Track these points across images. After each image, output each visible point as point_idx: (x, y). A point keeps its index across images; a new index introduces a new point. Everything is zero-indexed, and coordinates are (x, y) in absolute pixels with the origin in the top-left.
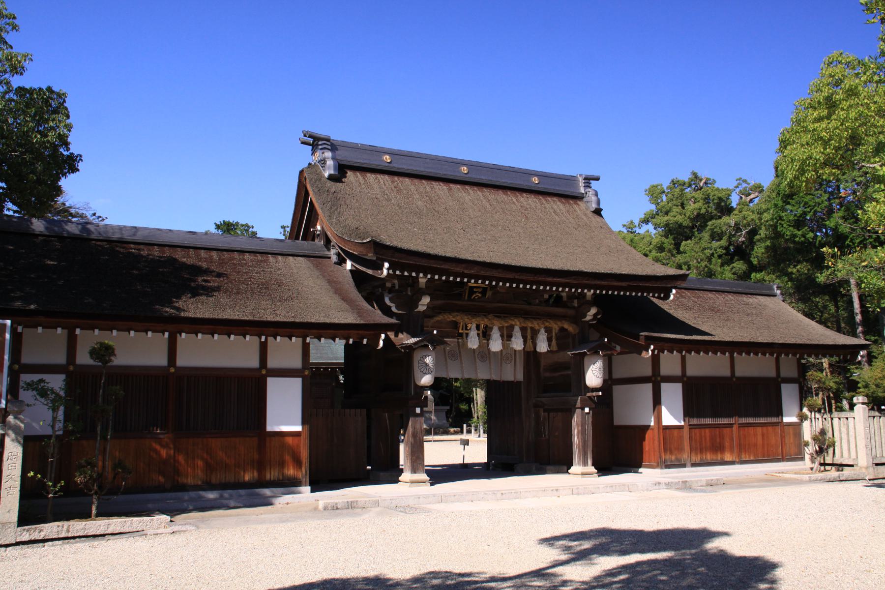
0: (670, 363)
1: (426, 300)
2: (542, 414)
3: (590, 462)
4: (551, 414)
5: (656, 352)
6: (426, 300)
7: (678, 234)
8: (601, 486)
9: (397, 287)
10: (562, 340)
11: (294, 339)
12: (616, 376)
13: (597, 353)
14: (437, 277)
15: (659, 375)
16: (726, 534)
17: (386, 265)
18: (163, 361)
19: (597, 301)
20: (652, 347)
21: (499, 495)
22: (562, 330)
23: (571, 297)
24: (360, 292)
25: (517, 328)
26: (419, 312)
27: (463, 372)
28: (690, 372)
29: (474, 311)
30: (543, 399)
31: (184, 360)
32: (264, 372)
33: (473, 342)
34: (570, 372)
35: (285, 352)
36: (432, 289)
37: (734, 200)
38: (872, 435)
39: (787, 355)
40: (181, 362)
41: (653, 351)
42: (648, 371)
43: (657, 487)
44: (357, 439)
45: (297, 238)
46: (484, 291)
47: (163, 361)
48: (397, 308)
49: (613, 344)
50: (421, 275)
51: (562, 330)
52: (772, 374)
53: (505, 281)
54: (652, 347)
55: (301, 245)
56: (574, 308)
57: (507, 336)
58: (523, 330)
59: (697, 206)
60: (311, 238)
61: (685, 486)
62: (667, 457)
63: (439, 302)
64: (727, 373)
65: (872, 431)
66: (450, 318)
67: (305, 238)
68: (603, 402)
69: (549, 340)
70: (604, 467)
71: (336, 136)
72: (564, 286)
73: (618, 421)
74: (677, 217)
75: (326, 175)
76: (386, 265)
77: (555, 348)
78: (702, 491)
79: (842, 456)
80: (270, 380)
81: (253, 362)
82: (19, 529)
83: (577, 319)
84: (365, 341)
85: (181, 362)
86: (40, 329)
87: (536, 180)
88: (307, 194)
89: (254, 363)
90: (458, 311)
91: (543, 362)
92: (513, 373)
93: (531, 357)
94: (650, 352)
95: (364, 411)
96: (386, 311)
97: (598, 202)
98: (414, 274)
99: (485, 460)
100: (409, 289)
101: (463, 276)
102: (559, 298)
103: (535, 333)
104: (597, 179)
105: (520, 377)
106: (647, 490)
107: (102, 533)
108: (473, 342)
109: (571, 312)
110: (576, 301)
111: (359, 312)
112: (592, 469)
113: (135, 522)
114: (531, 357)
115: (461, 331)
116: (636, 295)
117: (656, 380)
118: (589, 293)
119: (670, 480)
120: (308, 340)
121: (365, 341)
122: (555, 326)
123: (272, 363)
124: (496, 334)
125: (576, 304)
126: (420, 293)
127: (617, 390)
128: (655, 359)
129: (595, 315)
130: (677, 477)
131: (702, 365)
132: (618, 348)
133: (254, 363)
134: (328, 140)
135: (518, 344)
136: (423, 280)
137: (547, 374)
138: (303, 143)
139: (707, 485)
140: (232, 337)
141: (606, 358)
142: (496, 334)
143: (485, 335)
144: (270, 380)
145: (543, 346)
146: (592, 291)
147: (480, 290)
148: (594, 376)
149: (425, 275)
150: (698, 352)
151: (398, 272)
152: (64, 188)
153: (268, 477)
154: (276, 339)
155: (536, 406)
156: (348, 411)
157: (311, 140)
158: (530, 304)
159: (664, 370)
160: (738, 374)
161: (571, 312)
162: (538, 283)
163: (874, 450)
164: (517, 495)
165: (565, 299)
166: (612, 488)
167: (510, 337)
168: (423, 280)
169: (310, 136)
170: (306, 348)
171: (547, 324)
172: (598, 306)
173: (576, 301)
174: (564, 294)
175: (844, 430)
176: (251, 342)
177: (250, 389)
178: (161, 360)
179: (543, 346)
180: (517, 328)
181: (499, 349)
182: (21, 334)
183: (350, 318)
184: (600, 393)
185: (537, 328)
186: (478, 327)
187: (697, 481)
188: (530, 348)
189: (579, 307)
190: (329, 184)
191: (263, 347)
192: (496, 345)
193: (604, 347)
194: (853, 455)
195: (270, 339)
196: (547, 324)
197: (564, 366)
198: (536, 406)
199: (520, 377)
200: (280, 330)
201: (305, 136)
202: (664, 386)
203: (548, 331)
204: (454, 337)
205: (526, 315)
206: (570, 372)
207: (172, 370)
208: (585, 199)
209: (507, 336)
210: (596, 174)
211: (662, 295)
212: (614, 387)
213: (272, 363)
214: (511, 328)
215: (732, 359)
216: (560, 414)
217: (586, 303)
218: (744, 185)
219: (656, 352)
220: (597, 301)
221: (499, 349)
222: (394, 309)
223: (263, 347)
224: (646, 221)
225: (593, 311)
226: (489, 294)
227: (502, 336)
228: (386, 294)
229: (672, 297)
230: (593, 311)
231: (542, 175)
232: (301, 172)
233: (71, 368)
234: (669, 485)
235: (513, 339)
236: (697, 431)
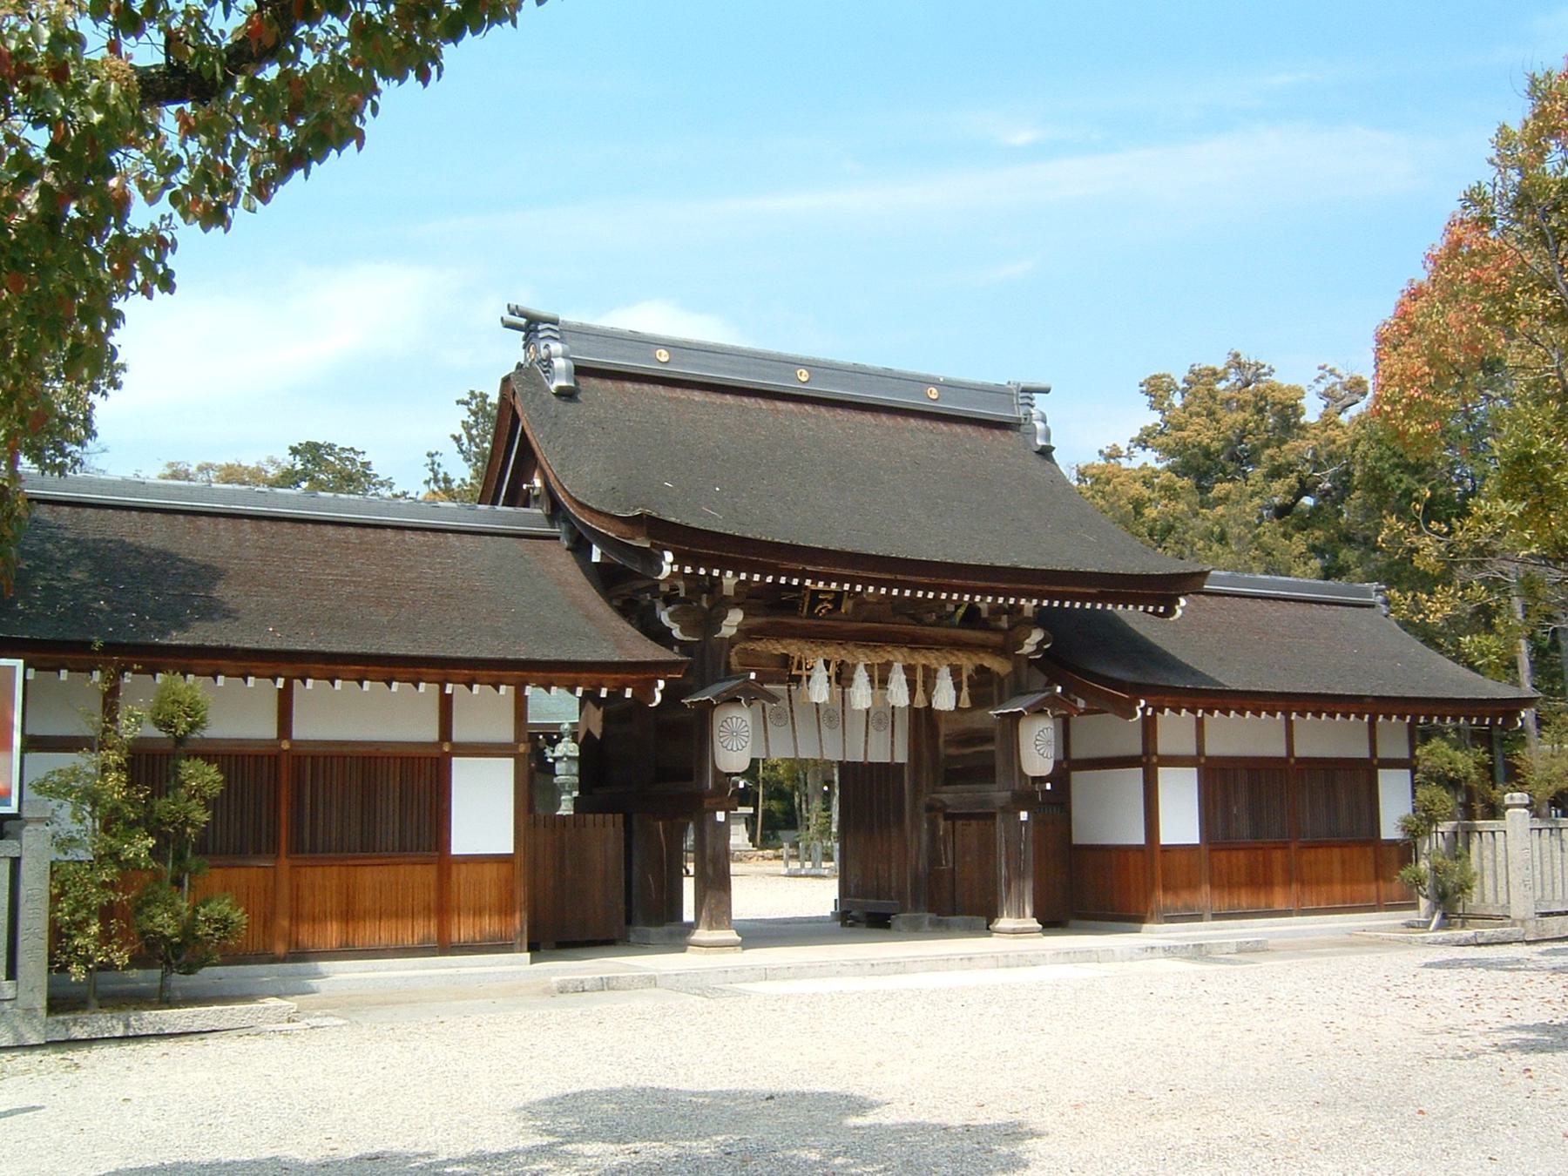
0: (1175, 732)
1: (735, 617)
2: (942, 823)
3: (1028, 911)
4: (959, 823)
5: (1149, 713)
6: (735, 617)
7: (1201, 468)
8: (1048, 954)
9: (682, 594)
10: (982, 688)
11: (422, 686)
12: (1078, 753)
13: (1042, 712)
17: (669, 557)
18: (269, 730)
19: (1042, 618)
20: (1143, 703)
21: (867, 967)
22: (981, 670)
23: (996, 611)
24: (609, 599)
25: (898, 667)
26: (723, 639)
28: (1211, 749)
29: (818, 636)
30: (944, 797)
31: (306, 729)
32: (446, 748)
33: (819, 690)
34: (991, 748)
35: (484, 712)
36: (746, 597)
37: (1312, 409)
38: (1537, 863)
39: (1388, 717)
41: (1144, 710)
42: (1136, 748)
43: (1148, 954)
44: (616, 865)
45: (494, 502)
46: (838, 597)
47: (269, 730)
48: (682, 631)
49: (1073, 696)
50: (729, 574)
51: (981, 670)
52: (1364, 753)
53: (878, 584)
54: (1143, 703)
55: (502, 515)
56: (1001, 630)
57: (881, 680)
58: (909, 670)
59: (1239, 417)
60: (521, 502)
61: (1199, 953)
62: (1169, 902)
63: (759, 621)
64: (1281, 751)
65: (1537, 854)
66: (778, 648)
67: (510, 502)
68: (1053, 799)
69: (958, 687)
70: (1053, 920)
71: (569, 316)
72: (984, 592)
73: (1077, 839)
74: (1202, 433)
75: (553, 387)
76: (669, 557)
77: (966, 703)
78: (1229, 962)
79: (1483, 901)
81: (428, 732)
82: (50, 1020)
83: (1007, 649)
84: (628, 693)
86: (64, 674)
87: (933, 393)
88: (516, 420)
89: (431, 733)
90: (793, 636)
91: (944, 729)
92: (887, 748)
93: (923, 720)
94: (1139, 713)
95: (620, 818)
96: (661, 636)
97: (1047, 436)
98: (716, 573)
100: (705, 596)
101: (803, 575)
102: (973, 609)
103: (930, 676)
104: (1046, 391)
105: (902, 757)
106: (1131, 959)
107: (185, 1029)
108: (819, 690)
109: (995, 638)
110: (1005, 617)
111: (619, 645)
112: (1033, 923)
113: (236, 1012)
114: (923, 720)
115: (794, 672)
117: (1148, 762)
118: (1029, 605)
119: (1173, 943)
120: (449, 689)
121: (628, 693)
122: (968, 663)
123: (459, 734)
124: (861, 677)
125: (1004, 622)
126: (722, 605)
127: (1081, 781)
128: (1149, 726)
129: (1040, 644)
130: (1186, 938)
131: (1244, 736)
132: (1081, 704)
133: (431, 733)
134: (555, 322)
135: (898, 693)
137: (952, 751)
138: (509, 326)
139: (1239, 951)
140: (310, 682)
141: (1060, 720)
142: (861, 677)
143: (842, 678)
145: (945, 698)
146: (1035, 602)
147: (830, 597)
148: (1037, 751)
149: (736, 574)
150: (1241, 712)
151: (688, 570)
152: (98, 422)
153: (455, 938)
154: (417, 687)
155: (930, 808)
156: (590, 817)
157: (523, 321)
158: (920, 622)
159: (1164, 746)
160: (1300, 751)
161: (995, 638)
162: (938, 589)
163: (1548, 888)
164: (899, 967)
165: (985, 614)
166: (1069, 956)
167: (884, 682)
169: (522, 316)
170: (521, 704)
171: (953, 659)
172: (1044, 627)
173: (1005, 617)
174: (983, 606)
175: (1487, 853)
176: (260, 691)
177: (422, 779)
179: (945, 698)
180: (898, 667)
181: (855, 708)
182: (451, 696)
183: (606, 653)
184: (1048, 786)
185: (934, 665)
186: (827, 664)
187: (1220, 945)
188: (920, 702)
189: (1011, 628)
190: (560, 405)
191: (285, 702)
192: (861, 695)
193: (1053, 701)
194: (1502, 896)
195: (297, 682)
196: (953, 659)
197: (983, 737)
198: (930, 808)
199: (902, 757)
201: (512, 313)
203: (956, 672)
204: (780, 682)
205: (914, 643)
206: (991, 748)
208: (1022, 428)
209: (881, 680)
210: (1043, 384)
211: (1161, 609)
214: (887, 667)
215: (1289, 724)
216: (974, 823)
217: (1021, 624)
218: (1334, 379)
219: (1149, 713)
220: (1042, 618)
221: (855, 708)
222: (677, 633)
223: (285, 702)
224: (1143, 442)
225: (1037, 635)
226: (847, 606)
227: (871, 681)
228: (659, 605)
229: (1179, 612)
230: (1037, 635)
231: (947, 386)
232: (506, 381)
234: (1170, 952)
235: (891, 686)
236: (1223, 855)
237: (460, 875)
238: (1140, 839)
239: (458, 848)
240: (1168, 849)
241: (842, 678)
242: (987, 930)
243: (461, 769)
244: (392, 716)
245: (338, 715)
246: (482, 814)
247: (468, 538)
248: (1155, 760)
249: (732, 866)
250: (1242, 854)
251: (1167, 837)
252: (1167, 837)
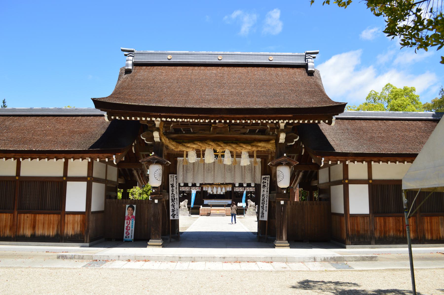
14: (306, 122)
15: (347, 179)
16: (294, 287)
27: (214, 179)
28: (375, 176)
31: (24, 173)
32: (65, 179)
33: (192, 158)
40: (23, 174)
80: (68, 183)
81: (60, 173)
85: (23, 174)
99: (257, 231)
116: (299, 122)
136: (282, 125)
143: (200, 154)
144: (68, 183)
159: (352, 175)
168: (282, 125)
176: (12, 162)
177: (58, 186)
178: (13, 173)
200: (382, 159)
202: (351, 187)
207: (17, 178)
212: (68, 182)
213: (70, 174)
233: (371, 181)
237: (69, 218)
238: (342, 212)
239: (68, 208)
240: (355, 216)
241: (200, 154)
242: (145, 246)
243: (70, 185)
244: (51, 168)
245: (33, 168)
246: (76, 199)
247: (362, 121)
248: (17, 178)
249: (10, 214)
250: (79, 216)
251: (353, 210)
252: (353, 210)
